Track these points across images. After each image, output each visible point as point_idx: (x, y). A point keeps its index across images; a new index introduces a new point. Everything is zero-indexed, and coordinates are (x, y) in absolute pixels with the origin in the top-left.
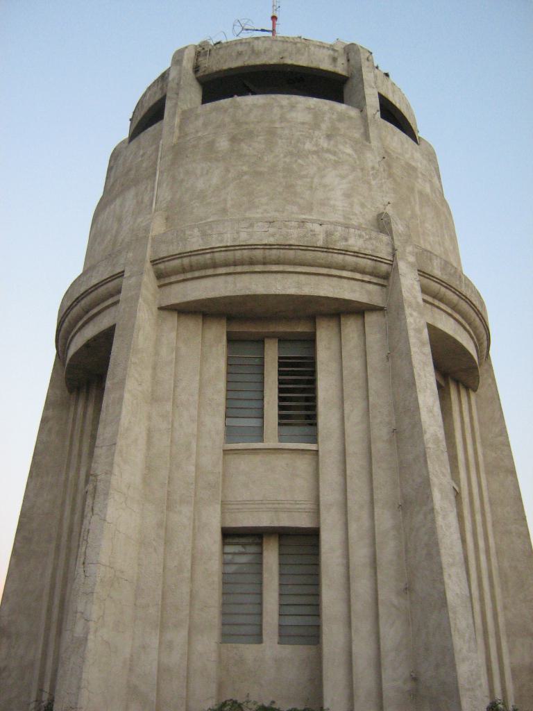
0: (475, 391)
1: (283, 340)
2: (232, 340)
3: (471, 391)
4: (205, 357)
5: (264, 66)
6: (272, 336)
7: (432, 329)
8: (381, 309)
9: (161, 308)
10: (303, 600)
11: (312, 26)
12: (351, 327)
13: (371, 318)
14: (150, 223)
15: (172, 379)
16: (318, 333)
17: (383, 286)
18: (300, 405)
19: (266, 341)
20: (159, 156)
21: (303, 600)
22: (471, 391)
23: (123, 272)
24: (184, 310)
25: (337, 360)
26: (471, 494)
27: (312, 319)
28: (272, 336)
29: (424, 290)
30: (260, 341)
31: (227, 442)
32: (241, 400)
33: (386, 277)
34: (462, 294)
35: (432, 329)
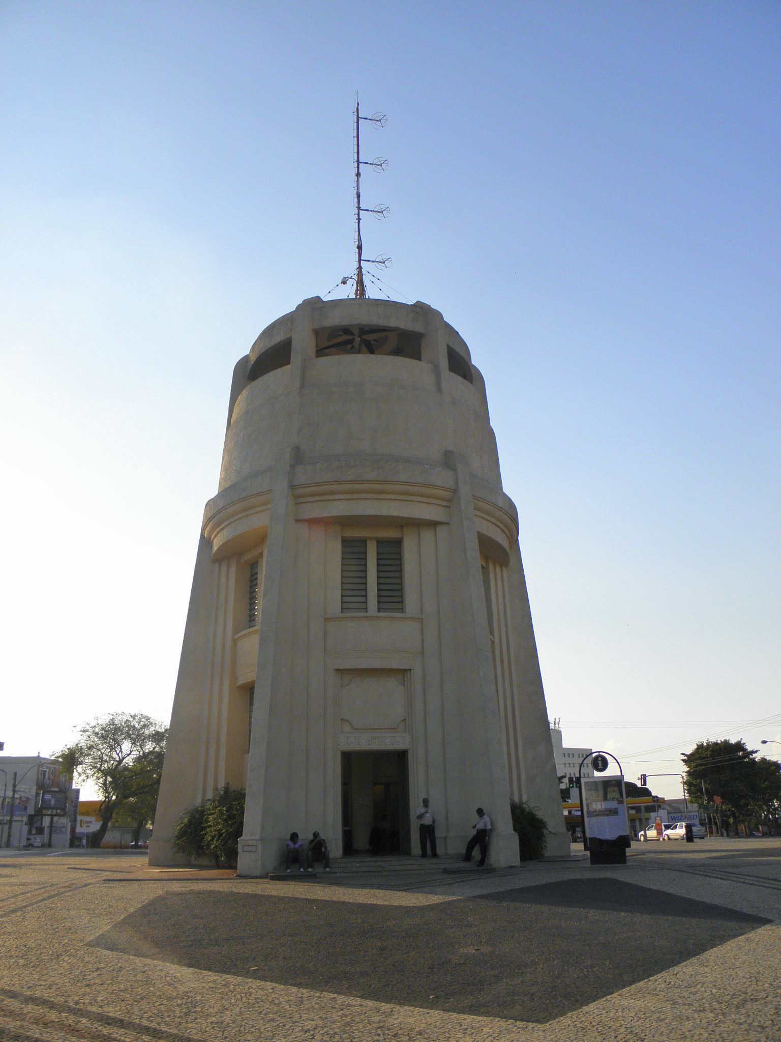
0: (507, 567)
2: (345, 542)
3: (504, 568)
7: (480, 536)
8: (448, 524)
9: (297, 521)
10: (357, 568)
12: (427, 536)
13: (442, 531)
16: (405, 540)
17: (449, 507)
18: (392, 596)
21: (357, 568)
22: (504, 568)
25: (417, 556)
26: (505, 706)
27: (401, 527)
28: (371, 538)
31: (408, 853)
32: (353, 592)
33: (451, 500)
35: (480, 536)
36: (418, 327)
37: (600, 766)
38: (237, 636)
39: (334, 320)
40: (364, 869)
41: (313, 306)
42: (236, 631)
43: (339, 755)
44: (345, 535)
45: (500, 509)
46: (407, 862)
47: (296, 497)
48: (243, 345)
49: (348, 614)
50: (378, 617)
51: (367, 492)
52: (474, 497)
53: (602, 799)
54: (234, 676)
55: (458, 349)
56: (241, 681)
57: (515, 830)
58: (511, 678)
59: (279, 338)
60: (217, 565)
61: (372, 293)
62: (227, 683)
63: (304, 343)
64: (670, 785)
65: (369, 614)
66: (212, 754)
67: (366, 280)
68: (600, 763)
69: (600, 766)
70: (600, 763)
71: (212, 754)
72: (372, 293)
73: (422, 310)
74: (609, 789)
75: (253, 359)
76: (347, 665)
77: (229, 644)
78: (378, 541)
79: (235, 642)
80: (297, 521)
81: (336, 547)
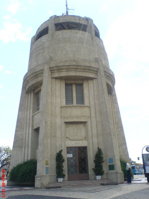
1: (76, 85)
2: (66, 84)
4: (60, 89)
5: (61, 197)
6: (74, 84)
11: (79, 11)
12: (91, 82)
14: (88, 79)
15: (54, 94)
17: (97, 74)
18: (81, 100)
19: (73, 85)
20: (116, 130)
23: (43, 70)
24: (56, 78)
28: (74, 84)
29: (105, 75)
30: (71, 85)
32: (69, 99)
34: (88, 72)
38: (33, 114)
39: (61, 21)
40: (75, 184)
41: (56, 17)
42: (33, 113)
43: (66, 149)
44: (66, 82)
46: (88, 182)
47: (51, 71)
49: (68, 105)
50: (77, 106)
51: (72, 69)
52: (104, 71)
53: (56, 23)
54: (33, 126)
55: (97, 31)
56: (35, 128)
57: (122, 171)
59: (46, 26)
60: (27, 94)
61: (69, 14)
63: (52, 28)
65: (74, 105)
66: (27, 135)
71: (27, 135)
72: (69, 14)
73: (87, 19)
76: (67, 121)
77: (31, 116)
79: (33, 116)
80: (51, 78)
81: (63, 85)
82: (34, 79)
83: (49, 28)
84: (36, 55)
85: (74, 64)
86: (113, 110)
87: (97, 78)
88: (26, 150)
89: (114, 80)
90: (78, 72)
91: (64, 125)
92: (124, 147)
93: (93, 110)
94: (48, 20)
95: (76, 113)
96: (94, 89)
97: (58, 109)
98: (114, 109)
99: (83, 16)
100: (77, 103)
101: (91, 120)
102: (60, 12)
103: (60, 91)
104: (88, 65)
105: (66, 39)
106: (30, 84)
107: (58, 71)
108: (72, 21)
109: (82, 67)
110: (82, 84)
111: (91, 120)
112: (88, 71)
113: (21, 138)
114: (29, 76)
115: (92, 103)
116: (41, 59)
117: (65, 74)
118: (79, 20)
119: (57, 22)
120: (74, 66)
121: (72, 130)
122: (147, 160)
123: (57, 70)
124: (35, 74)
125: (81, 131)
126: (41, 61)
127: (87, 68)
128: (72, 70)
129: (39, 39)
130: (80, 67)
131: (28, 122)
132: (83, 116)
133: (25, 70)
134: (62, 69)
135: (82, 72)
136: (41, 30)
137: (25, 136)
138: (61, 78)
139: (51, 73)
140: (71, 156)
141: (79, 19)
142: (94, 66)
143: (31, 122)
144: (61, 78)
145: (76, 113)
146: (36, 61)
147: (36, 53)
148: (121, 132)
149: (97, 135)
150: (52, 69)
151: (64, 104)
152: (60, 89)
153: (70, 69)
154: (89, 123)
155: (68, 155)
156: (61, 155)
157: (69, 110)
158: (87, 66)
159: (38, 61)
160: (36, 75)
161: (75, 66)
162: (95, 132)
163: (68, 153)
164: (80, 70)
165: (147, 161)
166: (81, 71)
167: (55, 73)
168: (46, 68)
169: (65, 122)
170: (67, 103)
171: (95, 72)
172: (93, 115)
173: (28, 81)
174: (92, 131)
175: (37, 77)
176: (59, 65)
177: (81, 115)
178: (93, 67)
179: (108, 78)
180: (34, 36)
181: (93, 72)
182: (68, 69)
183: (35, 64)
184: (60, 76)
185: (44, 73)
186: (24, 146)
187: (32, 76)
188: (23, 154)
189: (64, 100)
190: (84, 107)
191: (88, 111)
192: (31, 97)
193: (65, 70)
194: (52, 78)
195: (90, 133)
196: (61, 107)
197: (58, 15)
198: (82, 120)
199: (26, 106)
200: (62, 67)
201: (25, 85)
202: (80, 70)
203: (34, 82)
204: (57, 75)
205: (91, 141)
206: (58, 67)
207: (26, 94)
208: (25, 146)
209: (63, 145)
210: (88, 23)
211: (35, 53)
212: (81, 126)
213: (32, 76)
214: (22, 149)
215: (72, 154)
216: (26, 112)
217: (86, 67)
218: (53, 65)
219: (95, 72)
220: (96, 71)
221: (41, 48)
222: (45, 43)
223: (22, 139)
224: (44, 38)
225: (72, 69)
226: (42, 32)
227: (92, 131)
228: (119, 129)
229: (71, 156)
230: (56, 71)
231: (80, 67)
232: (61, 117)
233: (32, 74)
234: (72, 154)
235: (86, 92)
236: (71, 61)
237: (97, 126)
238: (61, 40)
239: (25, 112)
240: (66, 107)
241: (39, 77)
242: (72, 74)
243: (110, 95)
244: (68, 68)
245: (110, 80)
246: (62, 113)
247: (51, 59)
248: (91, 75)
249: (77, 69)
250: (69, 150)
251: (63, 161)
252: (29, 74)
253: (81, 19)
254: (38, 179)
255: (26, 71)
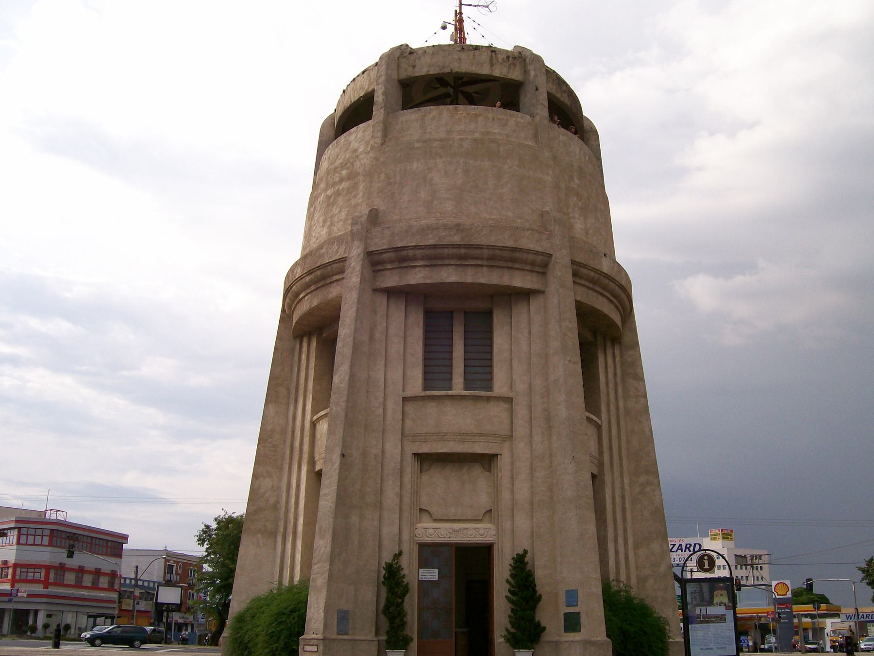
13: (535, 304)
18: (480, 372)
23: (343, 260)
24: (391, 293)
30: (449, 315)
32: (435, 371)
36: (515, 75)
37: (706, 567)
38: (315, 418)
39: (423, 69)
41: (401, 55)
42: (314, 412)
43: (416, 548)
45: (607, 276)
48: (329, 104)
53: (403, 76)
57: (608, 636)
58: (621, 465)
61: (473, 39)
62: (304, 469)
64: (200, 551)
67: (467, 26)
68: (706, 562)
69: (706, 567)
70: (706, 562)
72: (473, 39)
73: (522, 58)
74: (716, 593)
75: (339, 114)
76: (425, 449)
78: (465, 312)
80: (374, 290)
81: (417, 320)
82: (316, 289)
83: (376, 99)
84: (329, 197)
85: (457, 239)
86: (621, 404)
87: (543, 292)
88: (289, 546)
89: (623, 296)
90: (470, 268)
91: (410, 465)
92: (231, 580)
93: (521, 412)
94: (376, 64)
95: (456, 422)
96: (530, 333)
97: (393, 406)
98: (279, 488)
99: (506, 43)
100: (468, 384)
101: (512, 451)
102: (426, 32)
103: (405, 338)
104: (510, 243)
105: (436, 144)
106: (303, 308)
107: (396, 265)
108: (464, 71)
109: (486, 252)
110: (489, 314)
111: (512, 451)
112: (509, 265)
113: (272, 500)
114: (300, 278)
115: (521, 386)
116: (343, 214)
117: (421, 275)
118: (492, 65)
119: (407, 72)
120: (453, 246)
121: (439, 485)
122: (698, 600)
123: (391, 261)
124: (319, 273)
125: (477, 489)
126: (341, 223)
127: (506, 254)
128: (447, 262)
129: (342, 138)
130: (477, 252)
131: (297, 444)
132: (481, 435)
133: (286, 251)
134: (414, 259)
135: (485, 269)
136: (354, 99)
137: (284, 495)
138: (406, 295)
139: (374, 271)
140: (432, 575)
141: (491, 59)
142: (532, 246)
143: (306, 447)
144: (406, 295)
145: (456, 422)
146: (325, 221)
147: (329, 192)
148: (648, 489)
149: (532, 503)
150: (377, 258)
151: (416, 386)
152: (405, 333)
153: (443, 258)
154: (504, 461)
155: (421, 570)
156: (400, 569)
157: (432, 409)
158: (503, 248)
159: (332, 224)
160: (323, 278)
161: (459, 246)
162: (523, 493)
163: (424, 563)
164: (479, 262)
165: (698, 605)
166: (482, 266)
167: (387, 273)
168: (355, 253)
169: (421, 458)
170: (428, 384)
171: (537, 269)
172: (521, 429)
173: (297, 294)
174: (512, 491)
175: (328, 284)
176: (400, 245)
177: (475, 431)
178: (528, 251)
179: (591, 285)
180: (332, 117)
181: (528, 267)
182: (436, 258)
183: (322, 233)
184: (404, 283)
185: (348, 271)
186: (281, 529)
187: (308, 279)
188: (278, 561)
189: (417, 374)
190: (488, 399)
191: (505, 416)
192: (309, 354)
193: (421, 263)
194: (377, 290)
195: (506, 495)
196: (405, 399)
197: (414, 46)
198: (480, 448)
199: (293, 385)
200: (411, 253)
201: (290, 306)
202: (479, 262)
203: (315, 303)
204: (391, 280)
205: (507, 525)
206: (397, 249)
207: (295, 337)
208: (285, 528)
209: (406, 536)
210: (526, 72)
211: (326, 190)
212: (477, 471)
213: (308, 279)
214: (275, 542)
215: (436, 571)
216: (292, 408)
217: (498, 252)
218: (380, 242)
219: (537, 269)
220: (541, 264)
221: (344, 172)
222: (357, 156)
223: (275, 507)
224: (360, 136)
225: (450, 257)
226: (354, 114)
227: (512, 491)
228: (643, 479)
229: (432, 575)
230: (389, 266)
231: (477, 252)
232: (402, 434)
233: (309, 273)
234: (436, 571)
235: (500, 341)
236: (446, 227)
237: (532, 470)
238: (417, 145)
239: (288, 404)
240: (423, 398)
241: (334, 284)
242: (449, 276)
243: (613, 346)
244: (435, 255)
245: (601, 294)
246: (408, 422)
247: (374, 217)
248: (520, 280)
249: (465, 257)
250: (429, 553)
251: (406, 590)
252: (299, 272)
253: (500, 57)
254: (307, 648)
255: (297, 256)
